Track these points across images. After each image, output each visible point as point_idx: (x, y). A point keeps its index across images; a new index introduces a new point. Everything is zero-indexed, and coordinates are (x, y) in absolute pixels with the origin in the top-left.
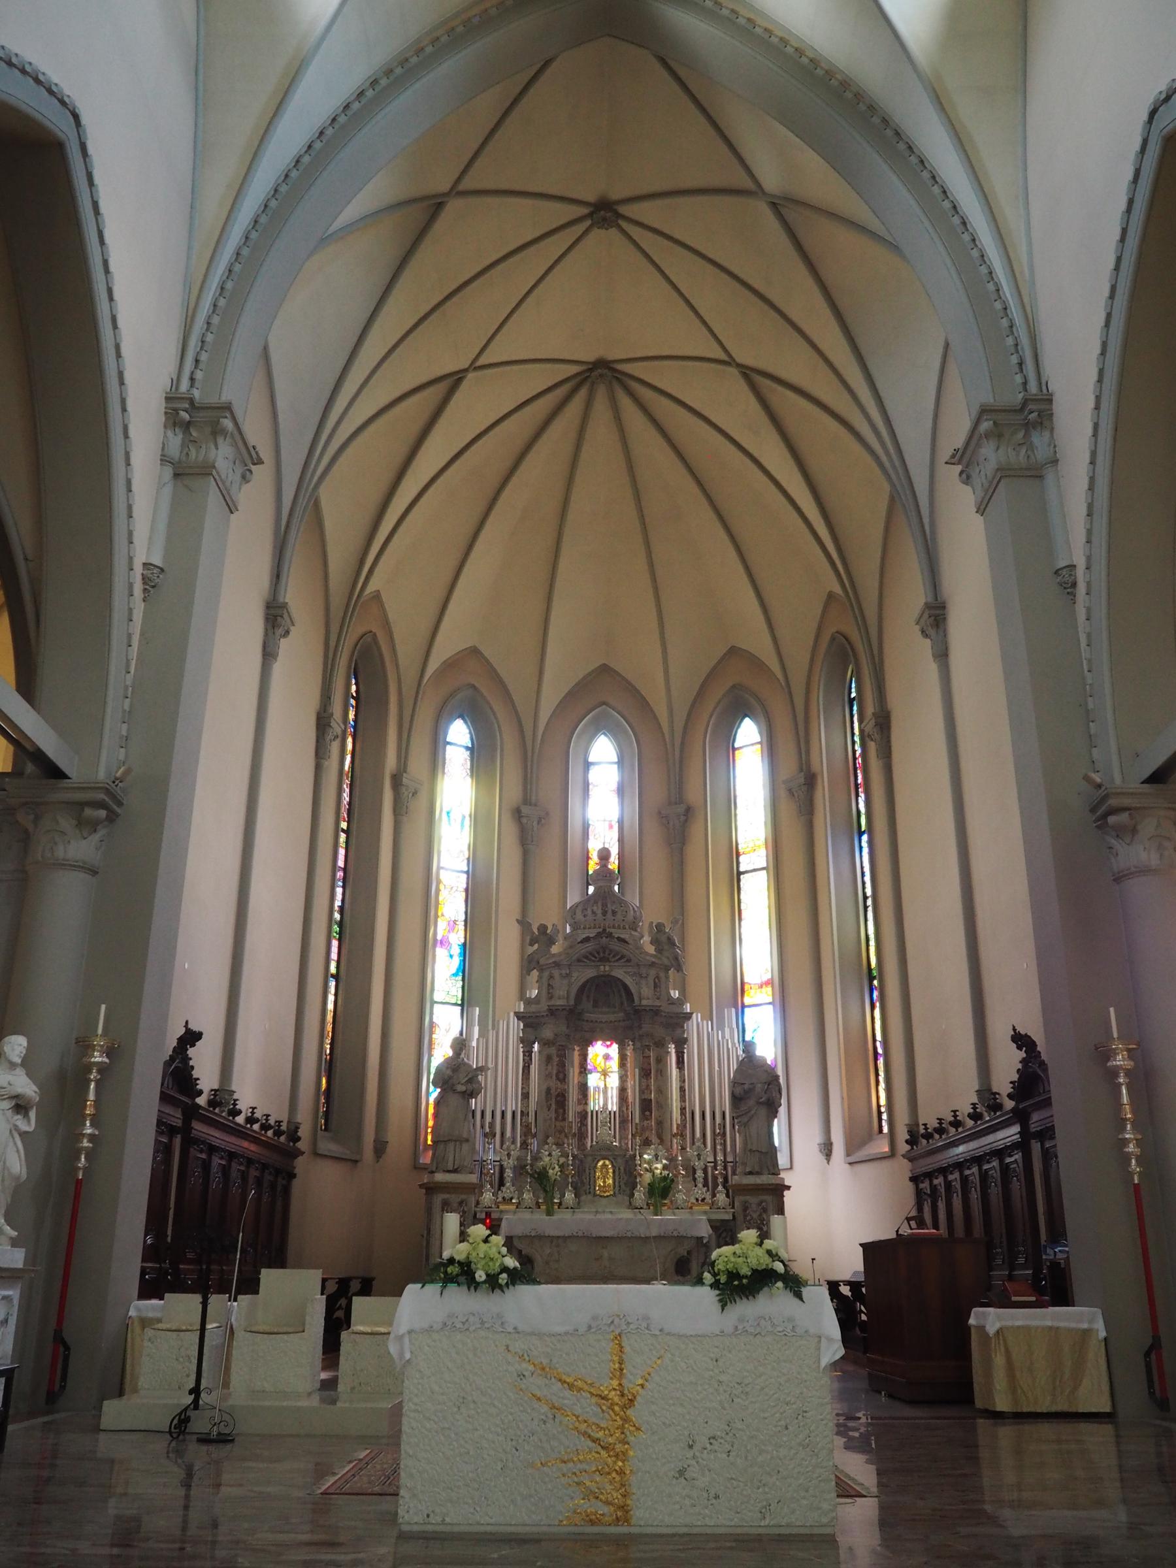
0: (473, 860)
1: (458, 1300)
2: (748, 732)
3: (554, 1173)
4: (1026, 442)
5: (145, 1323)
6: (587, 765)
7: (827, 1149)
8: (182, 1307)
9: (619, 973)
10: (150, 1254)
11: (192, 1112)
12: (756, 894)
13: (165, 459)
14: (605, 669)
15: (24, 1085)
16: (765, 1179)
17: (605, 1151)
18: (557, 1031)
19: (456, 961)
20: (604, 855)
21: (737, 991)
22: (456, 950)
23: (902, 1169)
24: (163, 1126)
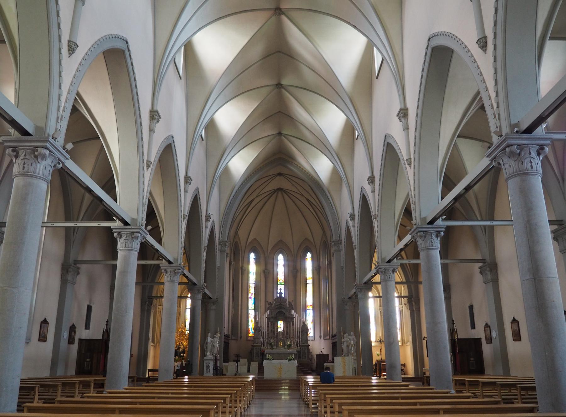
0: (256, 281)
1: (268, 361)
2: (309, 255)
4: (339, 246)
6: (278, 260)
7: (320, 337)
12: (310, 288)
14: (281, 241)
16: (306, 344)
17: (281, 340)
18: (273, 321)
19: (253, 301)
20: (281, 293)
21: (306, 306)
22: (253, 299)
23: (330, 341)
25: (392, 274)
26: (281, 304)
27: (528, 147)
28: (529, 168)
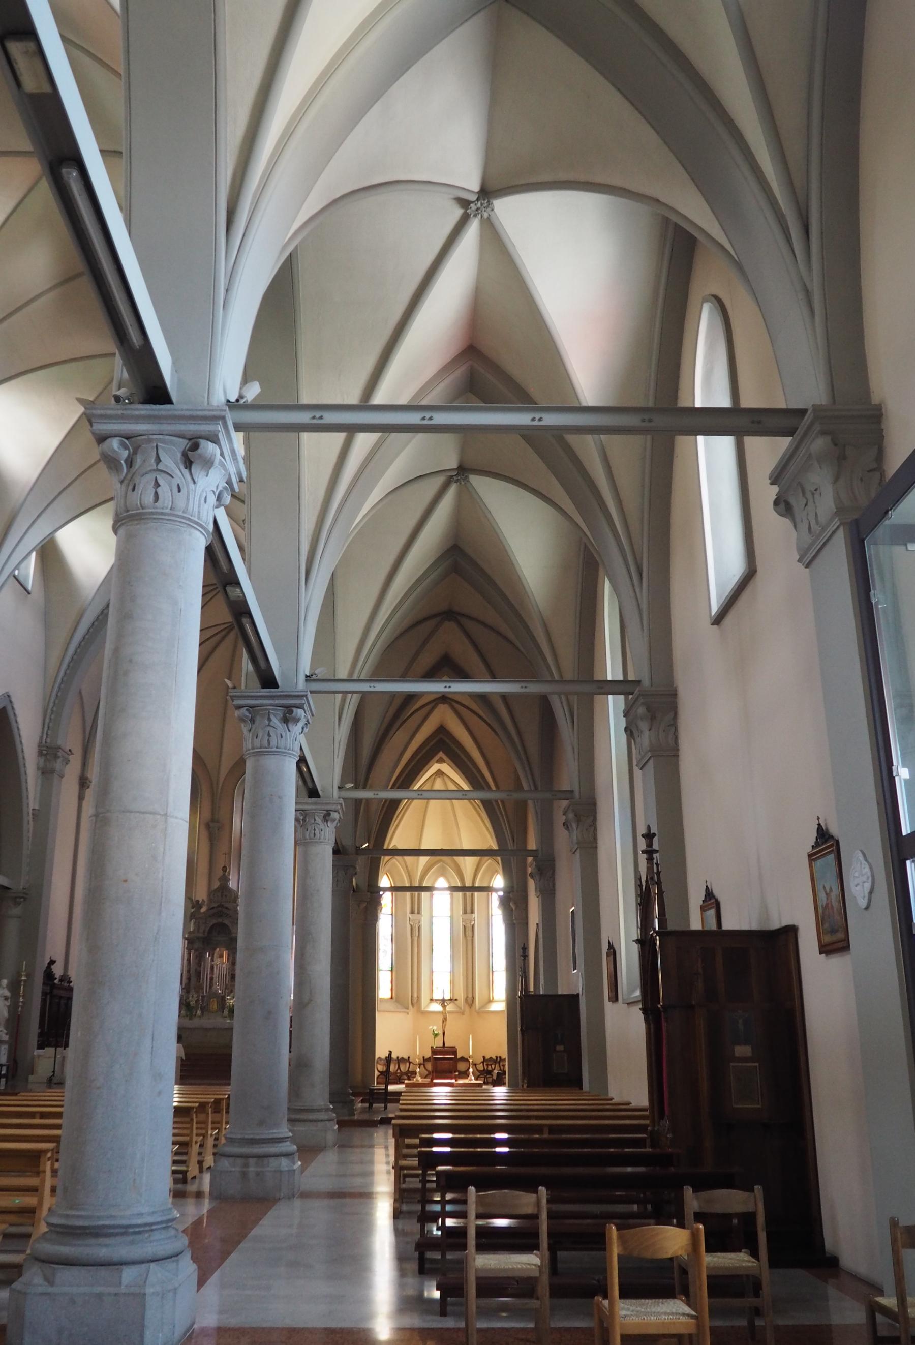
3: (193, 1003)
5: (39, 1056)
8: (50, 1051)
9: (226, 922)
10: (40, 1035)
11: (53, 986)
13: (38, 769)
15: (8, 994)
24: (44, 994)
25: (322, 826)
26: (221, 906)
27: (150, 441)
28: (149, 498)
